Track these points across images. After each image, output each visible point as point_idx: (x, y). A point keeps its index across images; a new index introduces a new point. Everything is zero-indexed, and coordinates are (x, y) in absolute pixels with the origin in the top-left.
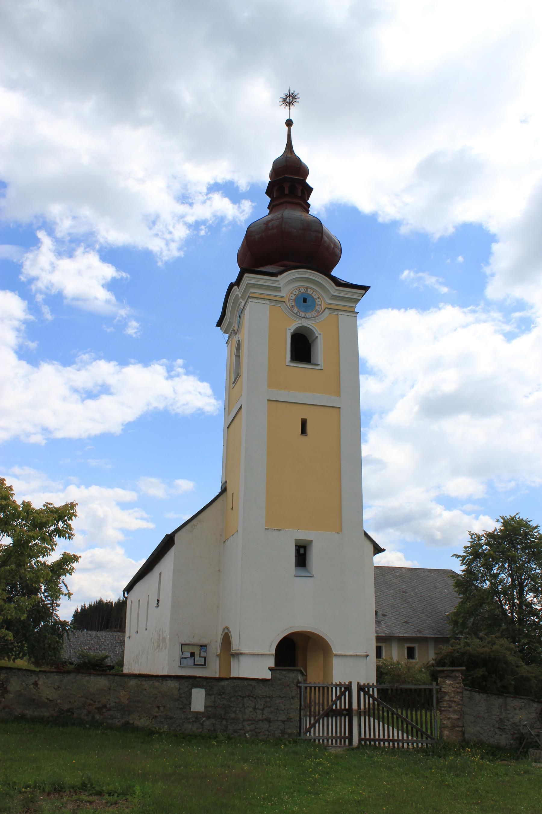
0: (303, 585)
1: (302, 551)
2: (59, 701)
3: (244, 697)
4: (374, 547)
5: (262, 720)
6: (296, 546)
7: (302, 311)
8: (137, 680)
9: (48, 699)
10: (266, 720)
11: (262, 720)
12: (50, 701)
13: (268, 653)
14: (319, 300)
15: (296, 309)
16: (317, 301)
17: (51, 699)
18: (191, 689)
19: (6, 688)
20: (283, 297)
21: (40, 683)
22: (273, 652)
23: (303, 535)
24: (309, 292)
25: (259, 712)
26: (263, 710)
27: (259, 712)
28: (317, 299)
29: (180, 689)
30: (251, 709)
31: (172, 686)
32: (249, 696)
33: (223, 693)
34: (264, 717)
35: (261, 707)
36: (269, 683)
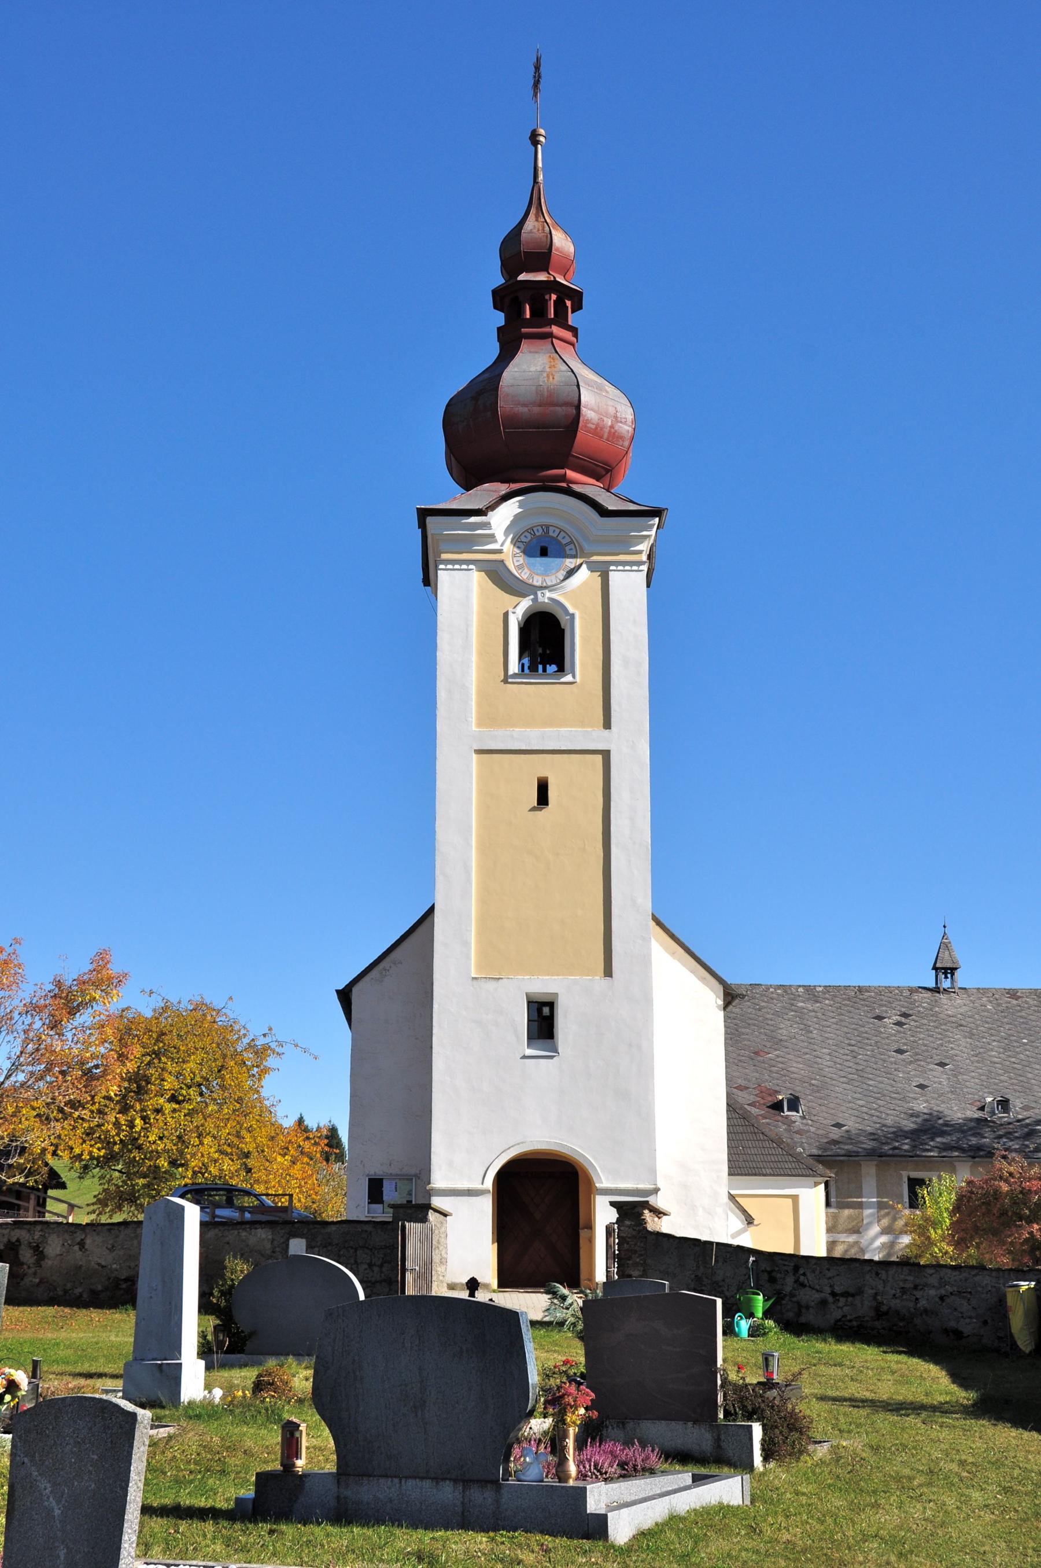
0: (544, 1070)
1: (546, 1011)
2: (114, 1266)
3: (356, 1250)
4: (720, 989)
5: (380, 1282)
6: (529, 1003)
7: (537, 574)
8: (217, 1230)
9: (99, 1264)
10: (385, 1280)
11: (380, 1282)
12: (103, 1267)
13: (476, 1185)
14: (572, 546)
15: (526, 570)
16: (567, 548)
17: (103, 1263)
18: (288, 1240)
19: (42, 1252)
20: (500, 551)
21: (88, 1241)
22: (489, 1184)
23: (542, 985)
24: (551, 534)
25: (376, 1269)
26: (381, 1266)
27: (376, 1269)
28: (567, 544)
29: (273, 1240)
30: (366, 1266)
31: (264, 1236)
32: (363, 1247)
33: (330, 1244)
34: (383, 1276)
35: (379, 1263)
36: (389, 1227)
